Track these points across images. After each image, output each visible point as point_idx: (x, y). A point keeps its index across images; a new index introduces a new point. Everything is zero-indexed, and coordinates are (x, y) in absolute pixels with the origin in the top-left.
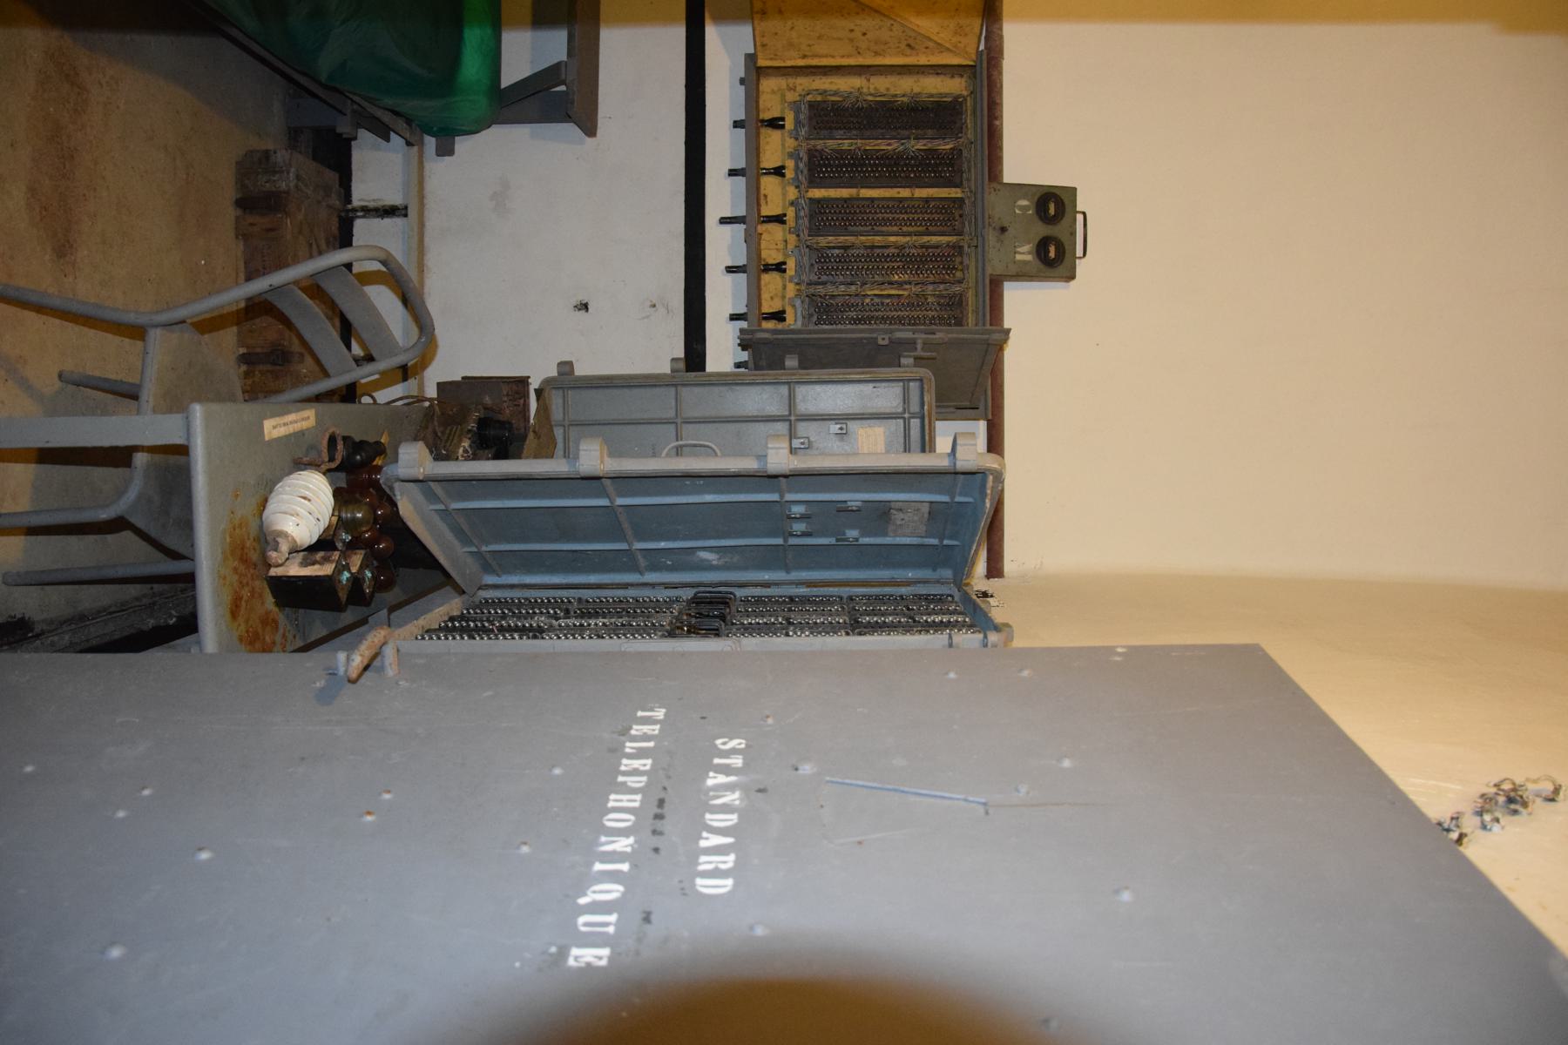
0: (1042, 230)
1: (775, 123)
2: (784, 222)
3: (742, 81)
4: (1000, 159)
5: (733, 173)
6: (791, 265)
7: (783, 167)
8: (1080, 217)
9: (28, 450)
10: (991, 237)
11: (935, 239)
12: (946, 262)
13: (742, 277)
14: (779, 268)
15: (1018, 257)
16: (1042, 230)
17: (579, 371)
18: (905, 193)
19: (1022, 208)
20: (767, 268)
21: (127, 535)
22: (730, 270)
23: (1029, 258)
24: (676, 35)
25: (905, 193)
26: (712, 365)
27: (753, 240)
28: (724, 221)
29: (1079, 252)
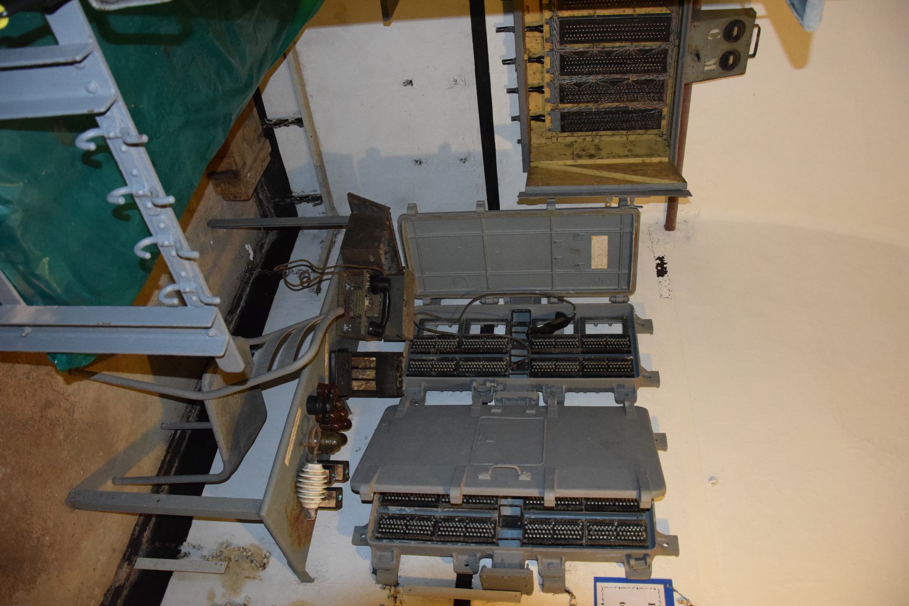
0: (726, 47)
1: (539, 118)
2: (542, 31)
3: (519, 142)
4: (686, 124)
5: (510, 91)
6: (547, 60)
7: (542, 26)
8: (756, 30)
9: (139, 357)
10: (689, 59)
11: (648, 45)
12: (659, 61)
13: (516, 96)
14: (539, 60)
15: (706, 68)
16: (726, 47)
17: (422, 209)
18: (628, 11)
19: (715, 35)
20: (531, 60)
21: (262, 525)
22: (505, 62)
23: (714, 67)
24: (466, 23)
25: (628, 11)
26: (504, 205)
27: (520, 44)
28: (499, 30)
29: (751, 52)
